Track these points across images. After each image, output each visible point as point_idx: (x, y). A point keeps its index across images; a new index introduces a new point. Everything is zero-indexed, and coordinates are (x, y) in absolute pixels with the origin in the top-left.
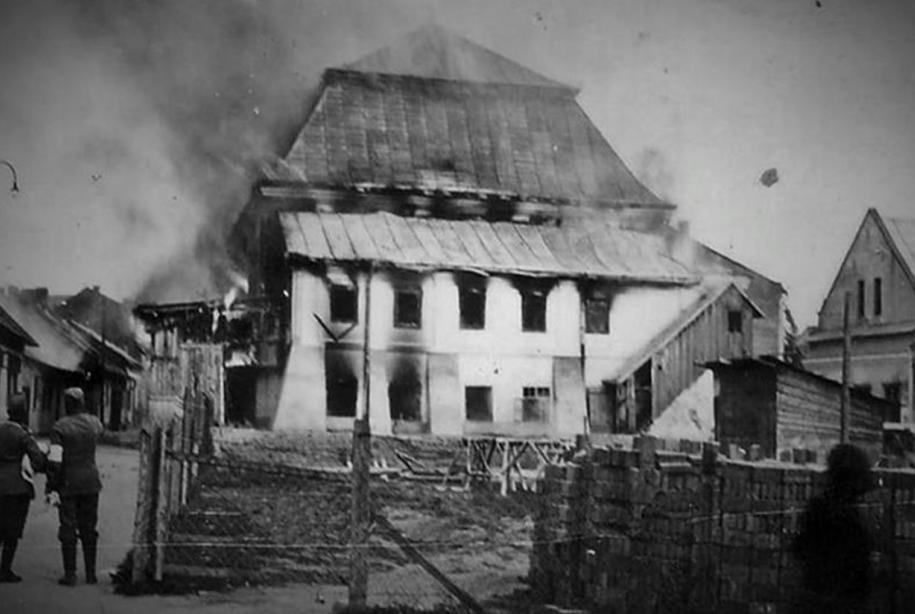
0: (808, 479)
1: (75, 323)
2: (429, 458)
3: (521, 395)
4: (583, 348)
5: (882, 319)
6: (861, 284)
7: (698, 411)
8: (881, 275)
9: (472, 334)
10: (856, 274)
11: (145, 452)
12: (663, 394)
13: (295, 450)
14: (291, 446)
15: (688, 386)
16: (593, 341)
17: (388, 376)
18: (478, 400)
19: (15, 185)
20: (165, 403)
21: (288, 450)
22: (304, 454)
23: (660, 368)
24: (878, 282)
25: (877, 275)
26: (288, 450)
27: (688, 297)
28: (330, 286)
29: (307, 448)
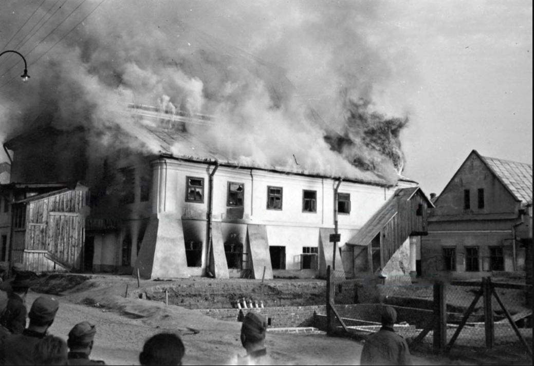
0: (180, 304)
1: (7, 148)
2: (287, 299)
3: (301, 252)
4: (336, 223)
5: (486, 210)
6: (467, 192)
7: (404, 263)
8: (484, 186)
9: (273, 213)
10: (462, 185)
11: (25, 198)
12: (386, 252)
13: (200, 295)
14: (197, 293)
15: (398, 247)
16: (341, 217)
17: (223, 238)
18: (277, 254)
19: (26, 71)
20: (36, 255)
21: (195, 295)
22: (206, 299)
23: (384, 236)
24: (481, 191)
25: (479, 187)
26: (195, 295)
27: (390, 193)
28: (219, 165)
29: (208, 294)
